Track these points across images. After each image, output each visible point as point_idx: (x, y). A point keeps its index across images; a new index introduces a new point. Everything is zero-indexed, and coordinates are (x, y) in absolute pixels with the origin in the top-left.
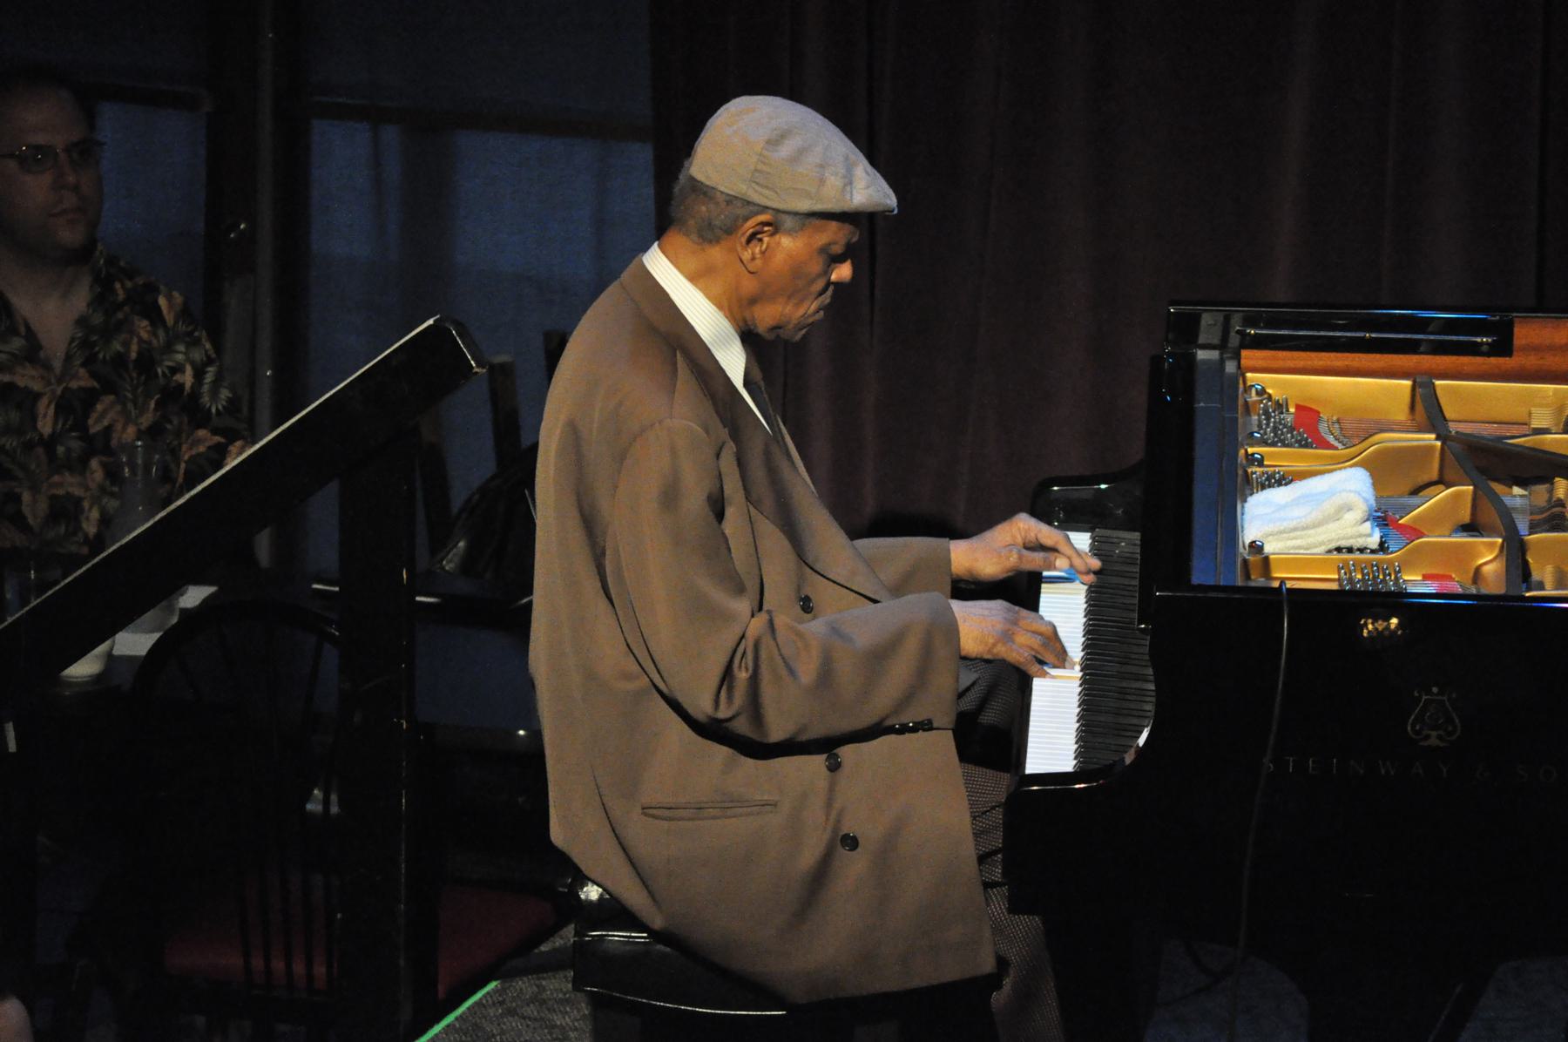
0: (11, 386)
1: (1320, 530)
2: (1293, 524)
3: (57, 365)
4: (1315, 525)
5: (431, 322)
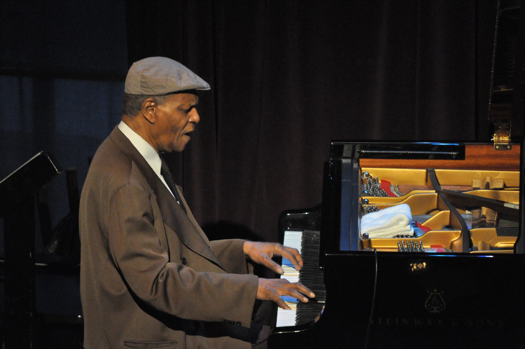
1: (390, 229)
2: (380, 226)
4: (389, 227)
5: (39, 154)
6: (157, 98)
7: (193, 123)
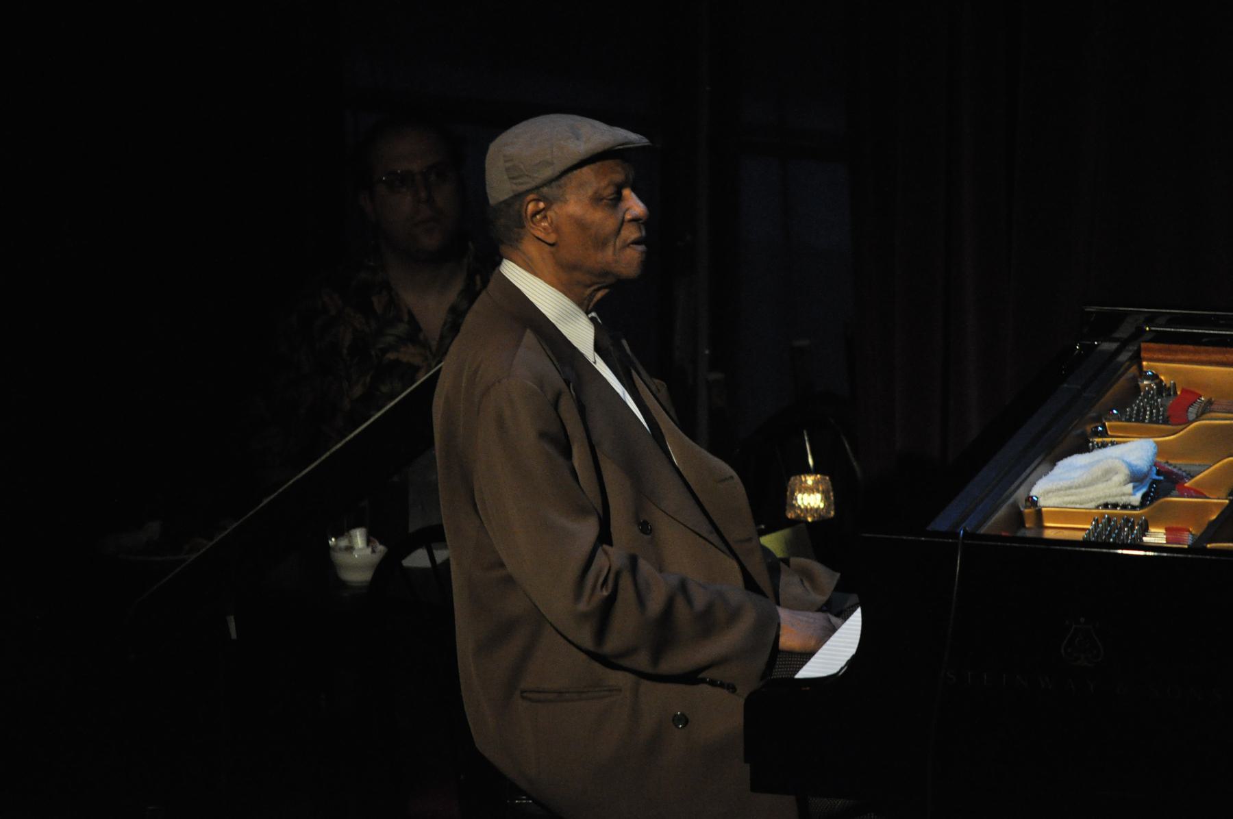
0: (397, 362)
1: (1091, 489)
3: (434, 344)
6: (545, 190)
7: (635, 220)
